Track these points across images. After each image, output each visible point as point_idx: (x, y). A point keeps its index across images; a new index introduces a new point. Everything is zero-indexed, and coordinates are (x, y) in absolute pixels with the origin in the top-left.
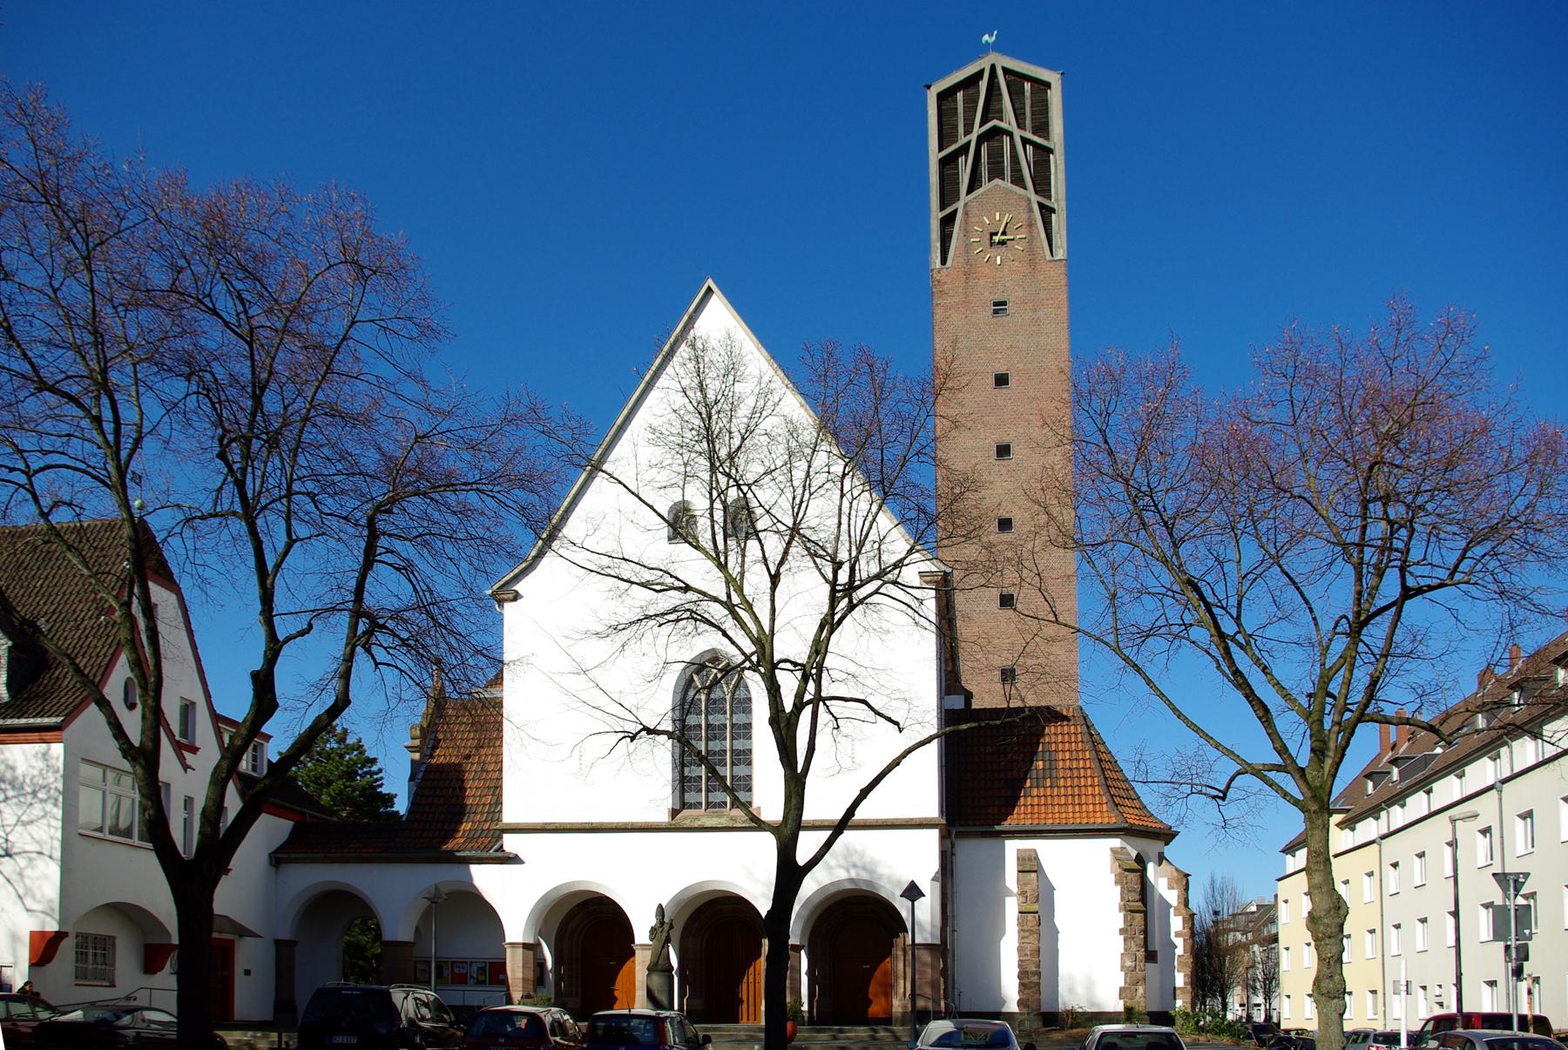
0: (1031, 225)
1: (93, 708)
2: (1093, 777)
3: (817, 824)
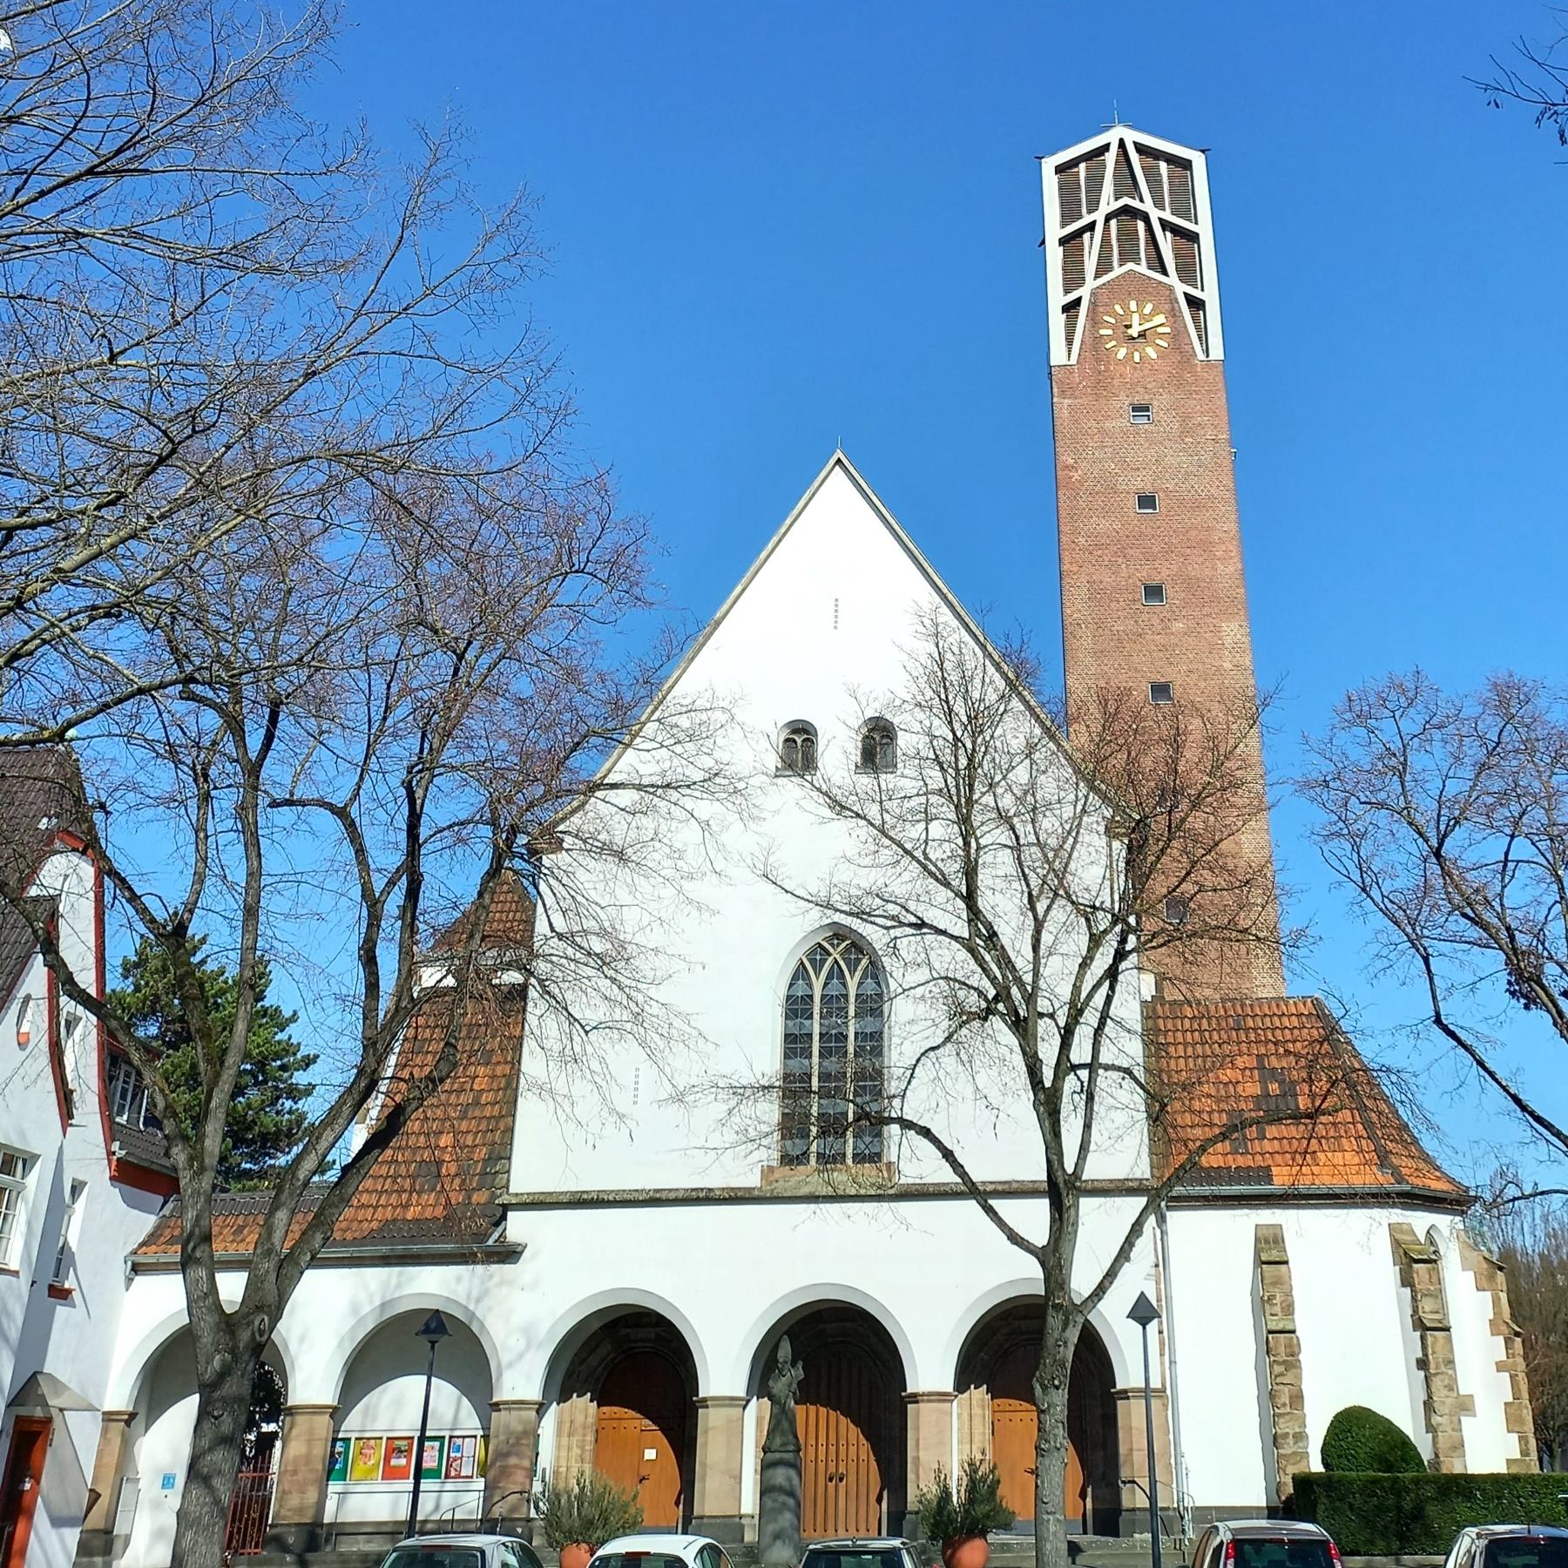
1: (425, 1377)
3: (664, 1196)
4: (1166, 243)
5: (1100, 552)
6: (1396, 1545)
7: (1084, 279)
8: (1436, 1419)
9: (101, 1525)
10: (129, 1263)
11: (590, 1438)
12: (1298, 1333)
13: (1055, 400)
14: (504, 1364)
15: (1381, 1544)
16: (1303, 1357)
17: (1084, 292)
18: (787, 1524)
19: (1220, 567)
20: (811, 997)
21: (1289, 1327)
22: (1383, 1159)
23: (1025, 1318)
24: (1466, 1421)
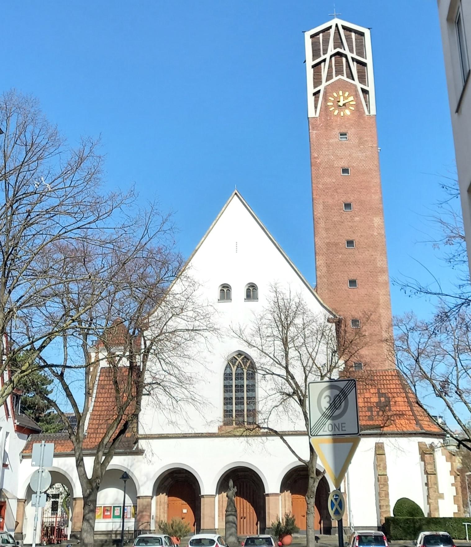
4: (354, 67)
5: (327, 191)
6: (413, 537)
7: (321, 82)
8: (430, 501)
9: (20, 532)
10: (21, 456)
11: (166, 506)
12: (388, 475)
13: (310, 131)
14: (140, 485)
15: (409, 537)
16: (389, 483)
17: (322, 88)
18: (233, 531)
19: (373, 196)
20: (232, 373)
21: (385, 474)
22: (417, 423)
23: (303, 471)
24: (440, 501)
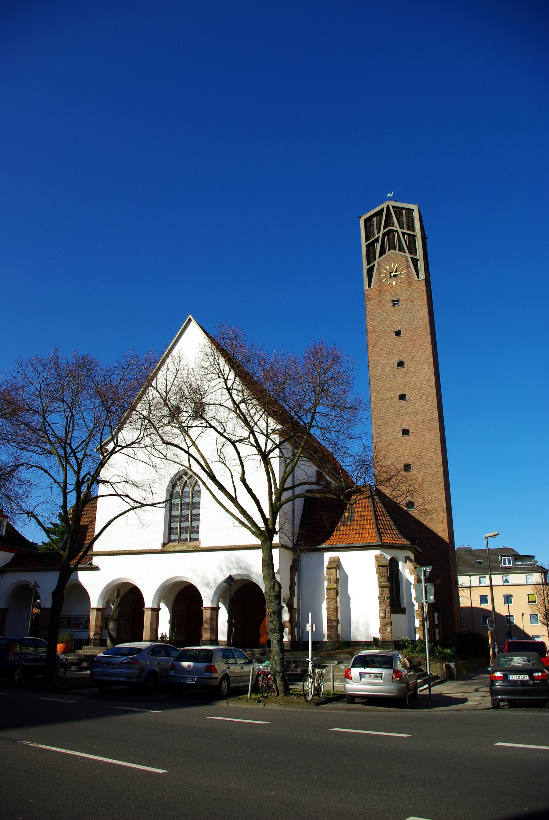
0: (408, 267)
2: (370, 520)
5: (381, 352)
